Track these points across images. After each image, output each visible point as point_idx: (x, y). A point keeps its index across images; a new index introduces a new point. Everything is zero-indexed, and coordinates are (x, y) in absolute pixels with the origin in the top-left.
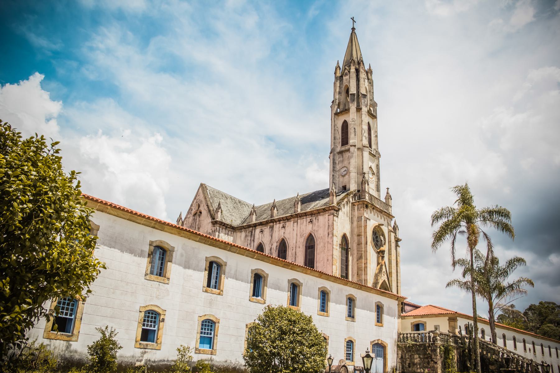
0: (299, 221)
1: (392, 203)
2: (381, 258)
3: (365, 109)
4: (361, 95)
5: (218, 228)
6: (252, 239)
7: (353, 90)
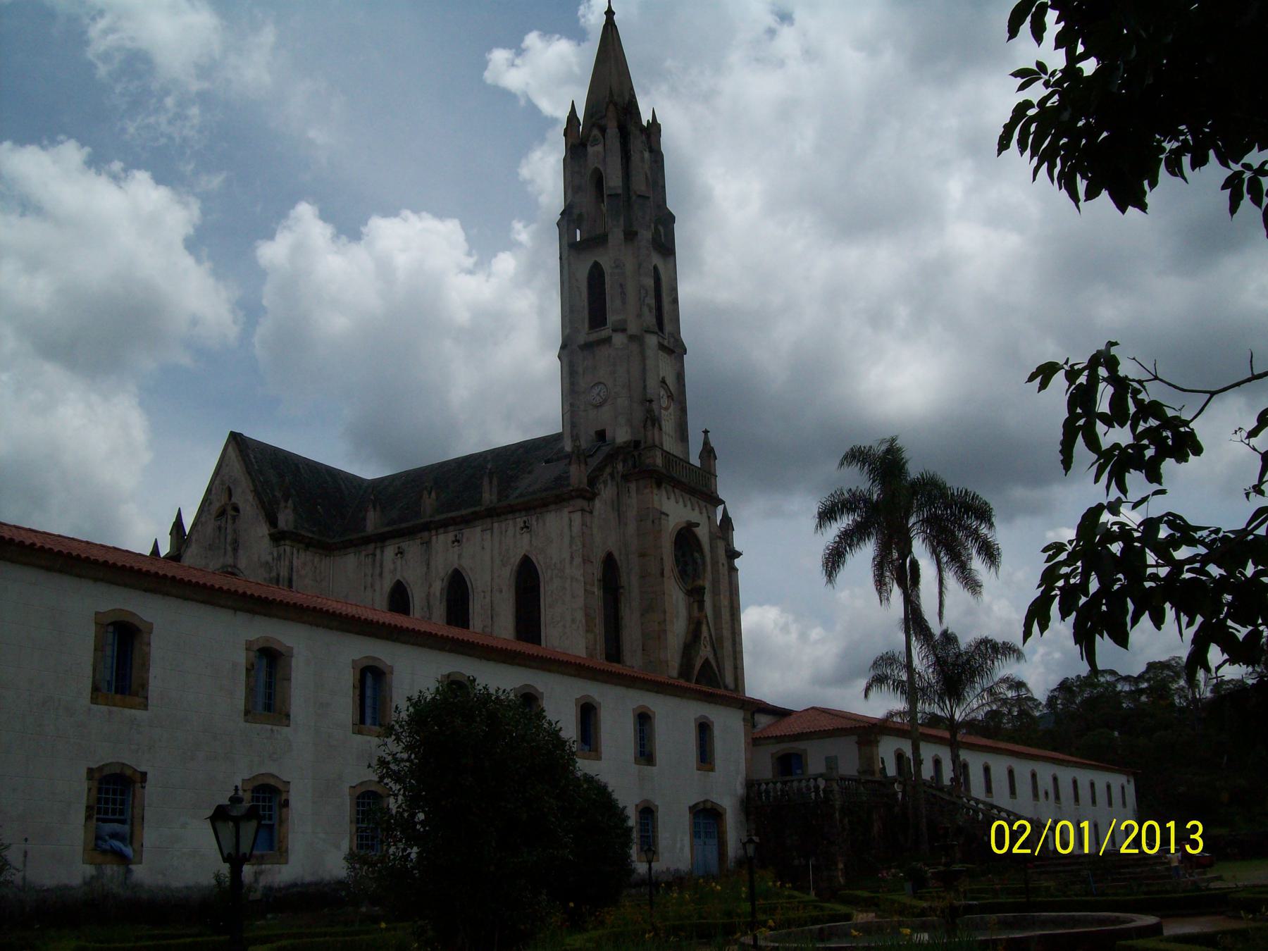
0: (496, 525)
1: (721, 468)
2: (696, 606)
3: (646, 235)
4: (634, 198)
5: (288, 549)
6: (377, 571)
7: (614, 180)
